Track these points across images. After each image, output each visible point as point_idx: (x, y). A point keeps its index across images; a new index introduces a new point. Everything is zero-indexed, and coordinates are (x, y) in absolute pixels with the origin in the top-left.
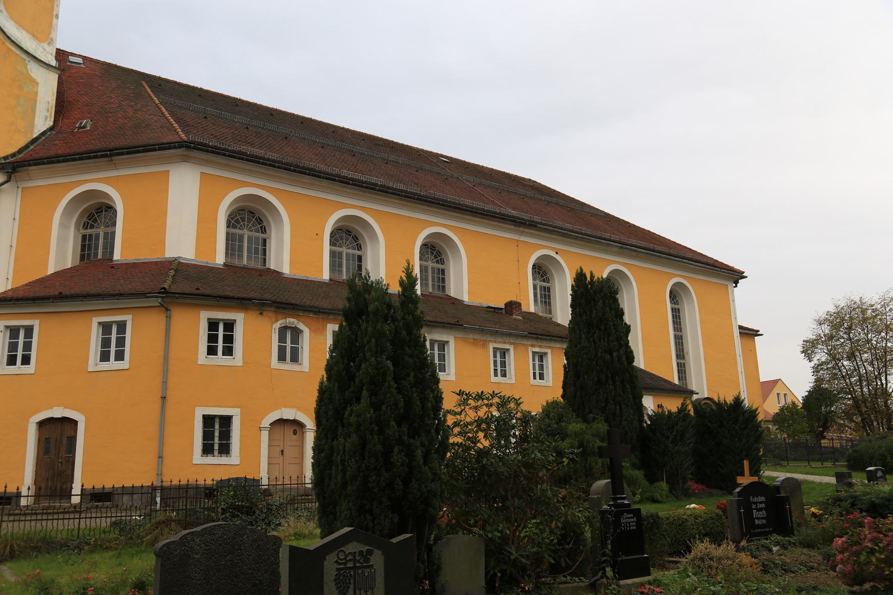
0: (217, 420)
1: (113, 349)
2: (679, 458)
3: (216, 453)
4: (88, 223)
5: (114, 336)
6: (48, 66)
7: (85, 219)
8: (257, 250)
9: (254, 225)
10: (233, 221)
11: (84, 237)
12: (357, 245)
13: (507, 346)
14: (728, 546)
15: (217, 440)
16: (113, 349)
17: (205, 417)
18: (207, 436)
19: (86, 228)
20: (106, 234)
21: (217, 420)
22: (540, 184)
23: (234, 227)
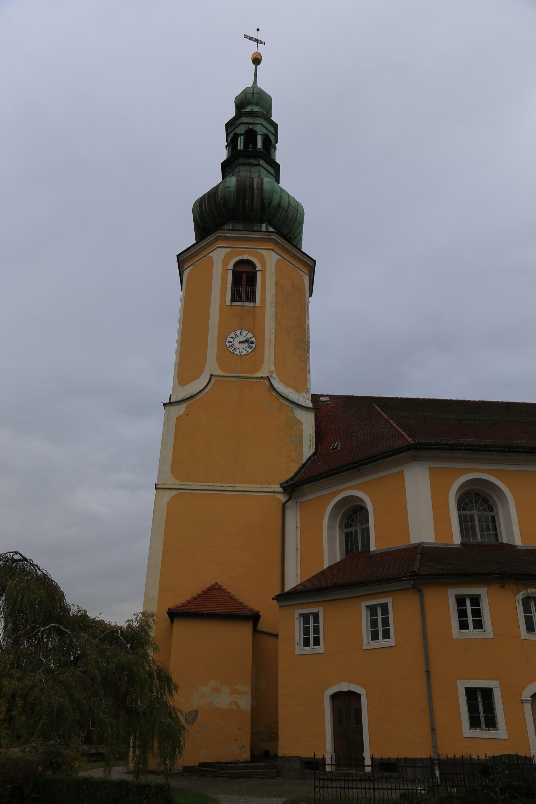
0: (479, 693)
3: (483, 726)
11: (346, 535)
12: (488, 506)
13: (314, 610)
15: (482, 713)
17: (467, 689)
18: (472, 708)
19: (347, 528)
20: (362, 530)
21: (479, 693)
23: (465, 509)
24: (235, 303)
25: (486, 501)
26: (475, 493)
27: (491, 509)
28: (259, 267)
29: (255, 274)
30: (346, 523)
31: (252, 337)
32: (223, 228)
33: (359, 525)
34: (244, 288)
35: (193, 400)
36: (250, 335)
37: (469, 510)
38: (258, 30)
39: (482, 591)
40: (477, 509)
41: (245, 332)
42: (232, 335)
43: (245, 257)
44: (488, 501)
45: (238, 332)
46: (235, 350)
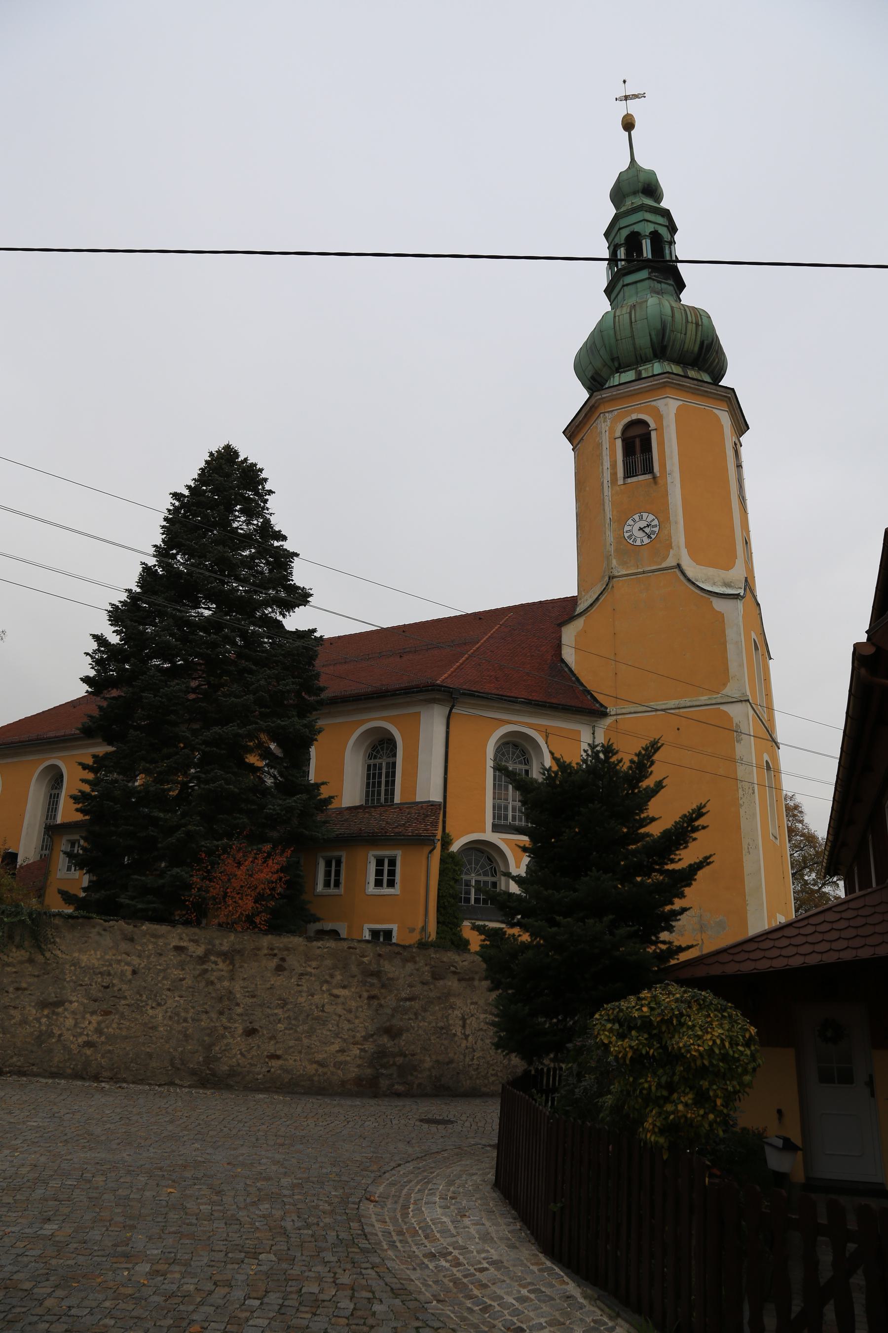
0: (382, 933)
1: (385, 878)
4: (372, 754)
5: (386, 868)
6: (782, 744)
7: (370, 751)
9: (518, 757)
11: (369, 766)
12: (524, 759)
14: (169, 990)
16: (385, 878)
19: (371, 759)
20: (388, 764)
21: (382, 933)
24: (629, 480)
25: (524, 752)
28: (653, 425)
29: (649, 434)
31: (654, 520)
32: (607, 386)
34: (639, 457)
35: (599, 603)
36: (651, 517)
38: (624, 82)
39: (398, 854)
41: (645, 515)
42: (630, 522)
43: (634, 417)
45: (636, 517)
46: (635, 541)
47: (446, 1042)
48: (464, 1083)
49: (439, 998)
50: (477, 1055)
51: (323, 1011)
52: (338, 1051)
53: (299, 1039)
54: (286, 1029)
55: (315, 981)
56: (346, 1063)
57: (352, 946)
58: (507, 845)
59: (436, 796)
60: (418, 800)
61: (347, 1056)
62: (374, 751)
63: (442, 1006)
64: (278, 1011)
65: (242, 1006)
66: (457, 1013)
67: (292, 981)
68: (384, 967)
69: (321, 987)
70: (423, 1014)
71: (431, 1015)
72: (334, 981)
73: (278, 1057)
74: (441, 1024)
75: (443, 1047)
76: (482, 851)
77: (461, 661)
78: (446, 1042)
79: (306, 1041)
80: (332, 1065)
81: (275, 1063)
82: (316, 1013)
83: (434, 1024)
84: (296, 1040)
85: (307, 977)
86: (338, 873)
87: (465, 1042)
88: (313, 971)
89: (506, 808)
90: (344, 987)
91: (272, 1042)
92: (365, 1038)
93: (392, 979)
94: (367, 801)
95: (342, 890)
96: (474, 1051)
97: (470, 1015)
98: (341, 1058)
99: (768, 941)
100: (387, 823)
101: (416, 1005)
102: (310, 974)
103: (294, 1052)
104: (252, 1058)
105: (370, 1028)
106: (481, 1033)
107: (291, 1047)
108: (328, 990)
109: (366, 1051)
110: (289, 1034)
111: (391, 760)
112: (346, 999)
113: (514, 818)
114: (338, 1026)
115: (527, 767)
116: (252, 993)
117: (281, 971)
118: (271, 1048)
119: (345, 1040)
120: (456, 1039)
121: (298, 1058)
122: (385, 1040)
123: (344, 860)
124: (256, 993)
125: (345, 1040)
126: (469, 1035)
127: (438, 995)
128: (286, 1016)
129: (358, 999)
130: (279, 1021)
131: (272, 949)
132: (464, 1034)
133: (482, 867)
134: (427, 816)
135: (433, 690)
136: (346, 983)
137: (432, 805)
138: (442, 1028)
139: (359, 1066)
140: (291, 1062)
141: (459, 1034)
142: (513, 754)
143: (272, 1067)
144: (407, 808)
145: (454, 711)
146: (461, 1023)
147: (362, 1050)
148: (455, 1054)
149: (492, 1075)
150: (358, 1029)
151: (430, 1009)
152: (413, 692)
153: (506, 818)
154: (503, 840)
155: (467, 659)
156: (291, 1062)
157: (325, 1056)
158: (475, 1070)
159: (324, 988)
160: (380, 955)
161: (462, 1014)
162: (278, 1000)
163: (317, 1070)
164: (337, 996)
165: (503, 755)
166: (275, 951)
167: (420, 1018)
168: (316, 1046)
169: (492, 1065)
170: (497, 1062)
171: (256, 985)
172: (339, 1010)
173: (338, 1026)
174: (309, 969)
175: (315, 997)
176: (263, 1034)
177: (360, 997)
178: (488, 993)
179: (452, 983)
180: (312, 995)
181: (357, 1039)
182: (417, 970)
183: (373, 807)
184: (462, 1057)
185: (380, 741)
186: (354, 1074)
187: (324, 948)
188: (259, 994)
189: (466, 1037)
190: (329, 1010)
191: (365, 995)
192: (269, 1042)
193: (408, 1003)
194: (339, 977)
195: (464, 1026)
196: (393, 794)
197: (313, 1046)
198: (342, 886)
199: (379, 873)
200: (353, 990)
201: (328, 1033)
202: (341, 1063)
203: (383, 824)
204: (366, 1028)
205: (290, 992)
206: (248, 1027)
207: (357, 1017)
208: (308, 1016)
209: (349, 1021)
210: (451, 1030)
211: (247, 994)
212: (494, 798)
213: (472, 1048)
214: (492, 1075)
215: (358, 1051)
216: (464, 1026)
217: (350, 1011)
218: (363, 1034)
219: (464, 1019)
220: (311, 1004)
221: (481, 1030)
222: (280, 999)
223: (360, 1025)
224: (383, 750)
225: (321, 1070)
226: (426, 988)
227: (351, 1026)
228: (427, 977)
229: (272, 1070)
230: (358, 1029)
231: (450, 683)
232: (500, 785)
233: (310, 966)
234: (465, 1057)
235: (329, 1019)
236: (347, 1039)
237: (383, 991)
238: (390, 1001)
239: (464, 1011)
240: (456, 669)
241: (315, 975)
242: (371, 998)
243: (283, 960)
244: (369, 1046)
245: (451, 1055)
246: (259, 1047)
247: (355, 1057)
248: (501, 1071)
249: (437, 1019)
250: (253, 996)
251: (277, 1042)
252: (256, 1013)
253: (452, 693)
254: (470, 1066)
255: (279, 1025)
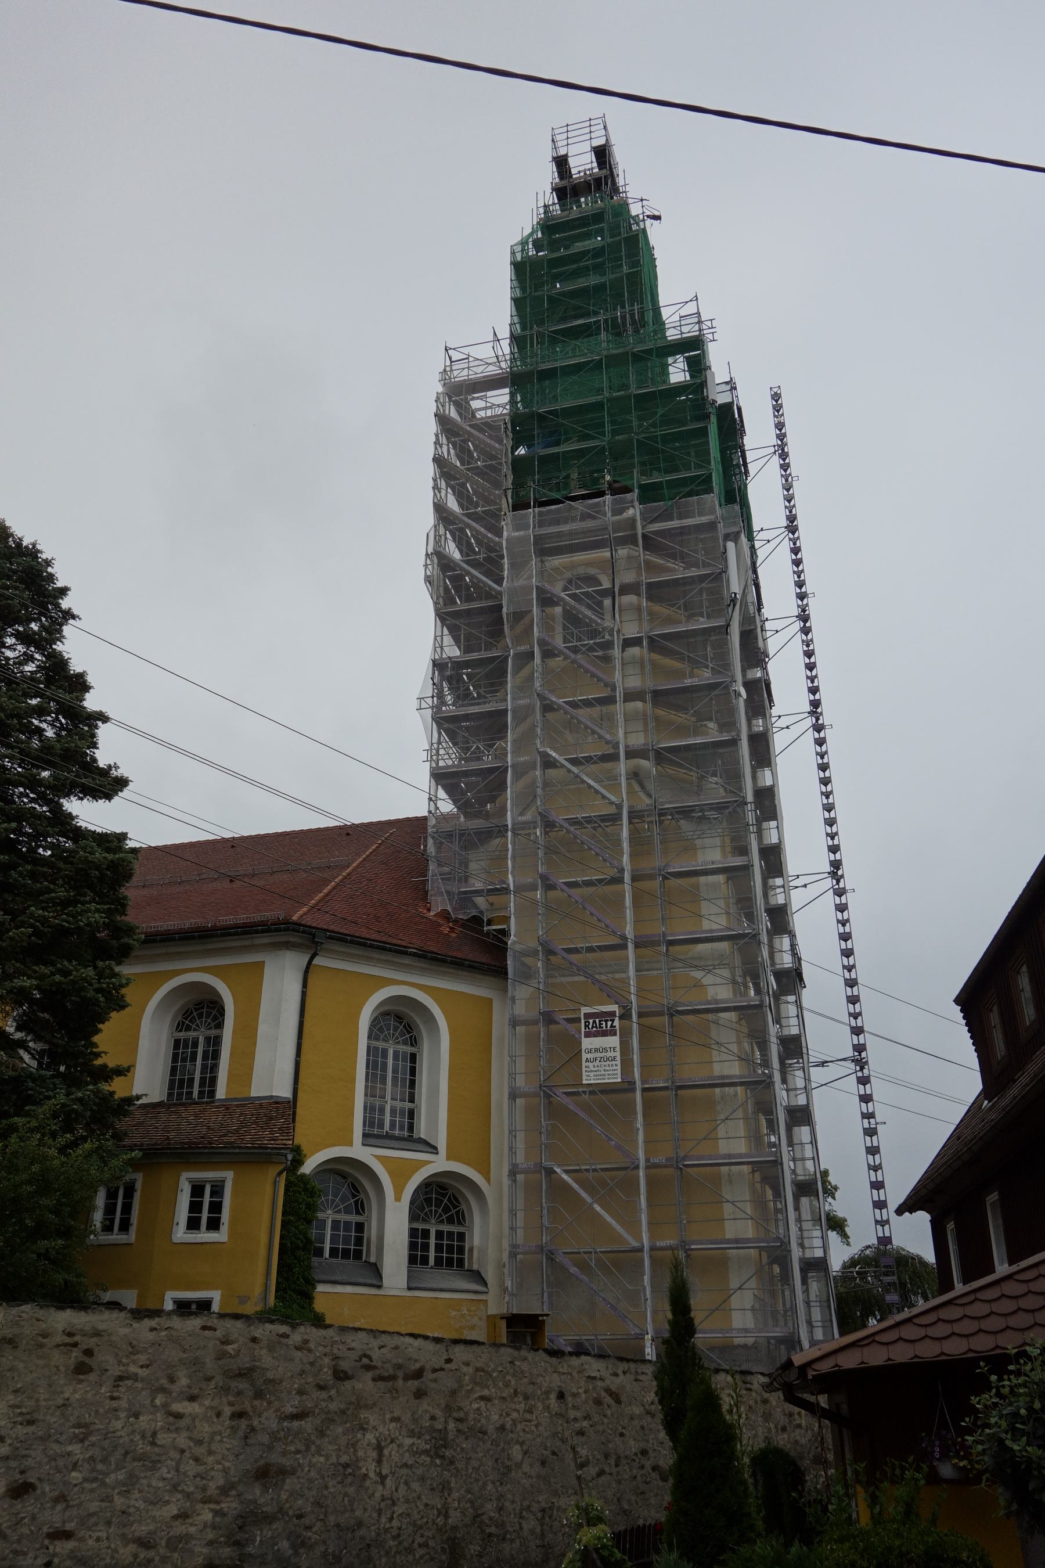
1: (205, 1215)
2: (616, 1375)
5: (207, 1199)
7: (180, 1018)
8: (404, 1080)
9: (402, 1035)
10: (376, 1030)
11: (177, 1043)
16: (205, 1215)
19: (181, 1031)
20: (208, 1039)
22: (1025, 890)
23: (377, 1039)
26: (438, 1186)
27: (414, 1041)
30: (179, 1022)
33: (202, 1030)
37: (384, 1040)
39: (228, 1176)
40: (438, 1218)
44: (459, 1202)
47: (351, 1490)
48: (378, 1562)
49: (343, 1412)
50: (399, 1509)
51: (153, 1444)
52: (176, 1517)
53: (108, 1499)
54: (85, 1480)
55: (143, 1389)
56: (187, 1538)
57: (209, 1324)
58: (382, 1163)
59: (284, 1091)
60: (253, 1094)
61: (191, 1525)
62: (186, 1019)
63: (348, 1425)
64: (75, 1448)
65: (9, 1441)
66: (370, 1437)
67: (103, 1390)
68: (260, 1360)
69: (152, 1401)
70: (318, 1442)
71: (330, 1443)
72: (175, 1388)
73: (67, 1535)
74: (345, 1459)
75: (346, 1499)
76: (344, 1176)
77: (325, 891)
78: (351, 1490)
79: (119, 1501)
80: (163, 1543)
81: (62, 1547)
82: (142, 1447)
83: (334, 1460)
84: (102, 1501)
85: (129, 1383)
86: (127, 1208)
87: (380, 1487)
88: (139, 1371)
89: (382, 1111)
90: (192, 1399)
91: (59, 1507)
92: (224, 1491)
93: (272, 1381)
94: (170, 1095)
95: (132, 1236)
96: (394, 1504)
97: (389, 1441)
98: (179, 1529)
99: (978, 1304)
100: (209, 1128)
101: (307, 1425)
102: (135, 1378)
103: (96, 1524)
104: (19, 1541)
105: (232, 1472)
106: (405, 1471)
107: (93, 1514)
108: (165, 1405)
109: (224, 1515)
110: (92, 1491)
111: (213, 1032)
112: (193, 1420)
113: (393, 1125)
114: (177, 1470)
115: (413, 1050)
116: (28, 1417)
117: (82, 1374)
118: (55, 1517)
119: (188, 1496)
120: (368, 1483)
121: (104, 1535)
122: (256, 1492)
123: (138, 1186)
124: (36, 1416)
125: (188, 1496)
126: (386, 1476)
127: (342, 1406)
128: (87, 1456)
129: (215, 1420)
130: (75, 1466)
131: (70, 1335)
132: (380, 1474)
133: (343, 1200)
134: (271, 1119)
135: (287, 930)
136: (196, 1391)
137: (277, 1103)
138: (346, 1466)
139: (210, 1543)
140: (91, 1542)
141: (372, 1475)
142: (396, 1029)
143: (55, 1555)
144: (237, 1106)
145: (315, 962)
146: (375, 1454)
147: (216, 1513)
148: (365, 1509)
149: (420, 1545)
150: (212, 1473)
151: (329, 1432)
152: (257, 932)
153: (381, 1125)
154: (378, 1157)
155: (334, 888)
156: (91, 1542)
157: (152, 1527)
158: (394, 1538)
159: (158, 1402)
160: (254, 1340)
161: (377, 1439)
162: (74, 1427)
163: (135, 1556)
164: (179, 1416)
165: (381, 1030)
166: (77, 1338)
167: (313, 1448)
168: (138, 1509)
169: (421, 1527)
170: (427, 1522)
171: (37, 1400)
172: (182, 1440)
173: (177, 1470)
174: (133, 1369)
175: (141, 1418)
176: (44, 1493)
177: (218, 1415)
178: (418, 1401)
179: (364, 1384)
180: (136, 1416)
181: (209, 1493)
182: (312, 1364)
183: (182, 1105)
184: (375, 1515)
185: (196, 1005)
186: (200, 1559)
187: (161, 1330)
188: (41, 1417)
189: (383, 1478)
190: (164, 1442)
191: (228, 1411)
192: (53, 1508)
193: (296, 1424)
194: (184, 1381)
195: (379, 1461)
196: (213, 1081)
197: (132, 1510)
198: (133, 1229)
199: (195, 1207)
200: (207, 1403)
201: (161, 1484)
202: (180, 1538)
203: (204, 1130)
204: (226, 1471)
205: (97, 1412)
206: (16, 1481)
207: (210, 1453)
208: (126, 1453)
209: (197, 1460)
210: (360, 1468)
211: (20, 1419)
212: (366, 1095)
213: (391, 1498)
214: (420, 1545)
215: (210, 1515)
216: (379, 1461)
217: (199, 1442)
218: (221, 1482)
219: (379, 1448)
220: (133, 1432)
221: (405, 1465)
222: (78, 1426)
223: (217, 1467)
224: (207, 1017)
225: (143, 1554)
226: (324, 1395)
227: (201, 1469)
228: (327, 1375)
229: (56, 1560)
230: (212, 1473)
231: (308, 921)
232: (374, 1075)
233: (134, 1362)
234: (379, 1515)
235: (163, 1458)
236: (192, 1493)
237: (257, 1403)
238: (269, 1421)
239: (381, 1434)
240: (320, 901)
241: (142, 1380)
242: (239, 1415)
243: (89, 1353)
244: (230, 1505)
245: (358, 1513)
246: (34, 1518)
247: (205, 1526)
248: (434, 1538)
249: (340, 1450)
250: (31, 1423)
251: (68, 1506)
252: (33, 1453)
253: (314, 936)
254: (387, 1530)
255: (74, 1474)
